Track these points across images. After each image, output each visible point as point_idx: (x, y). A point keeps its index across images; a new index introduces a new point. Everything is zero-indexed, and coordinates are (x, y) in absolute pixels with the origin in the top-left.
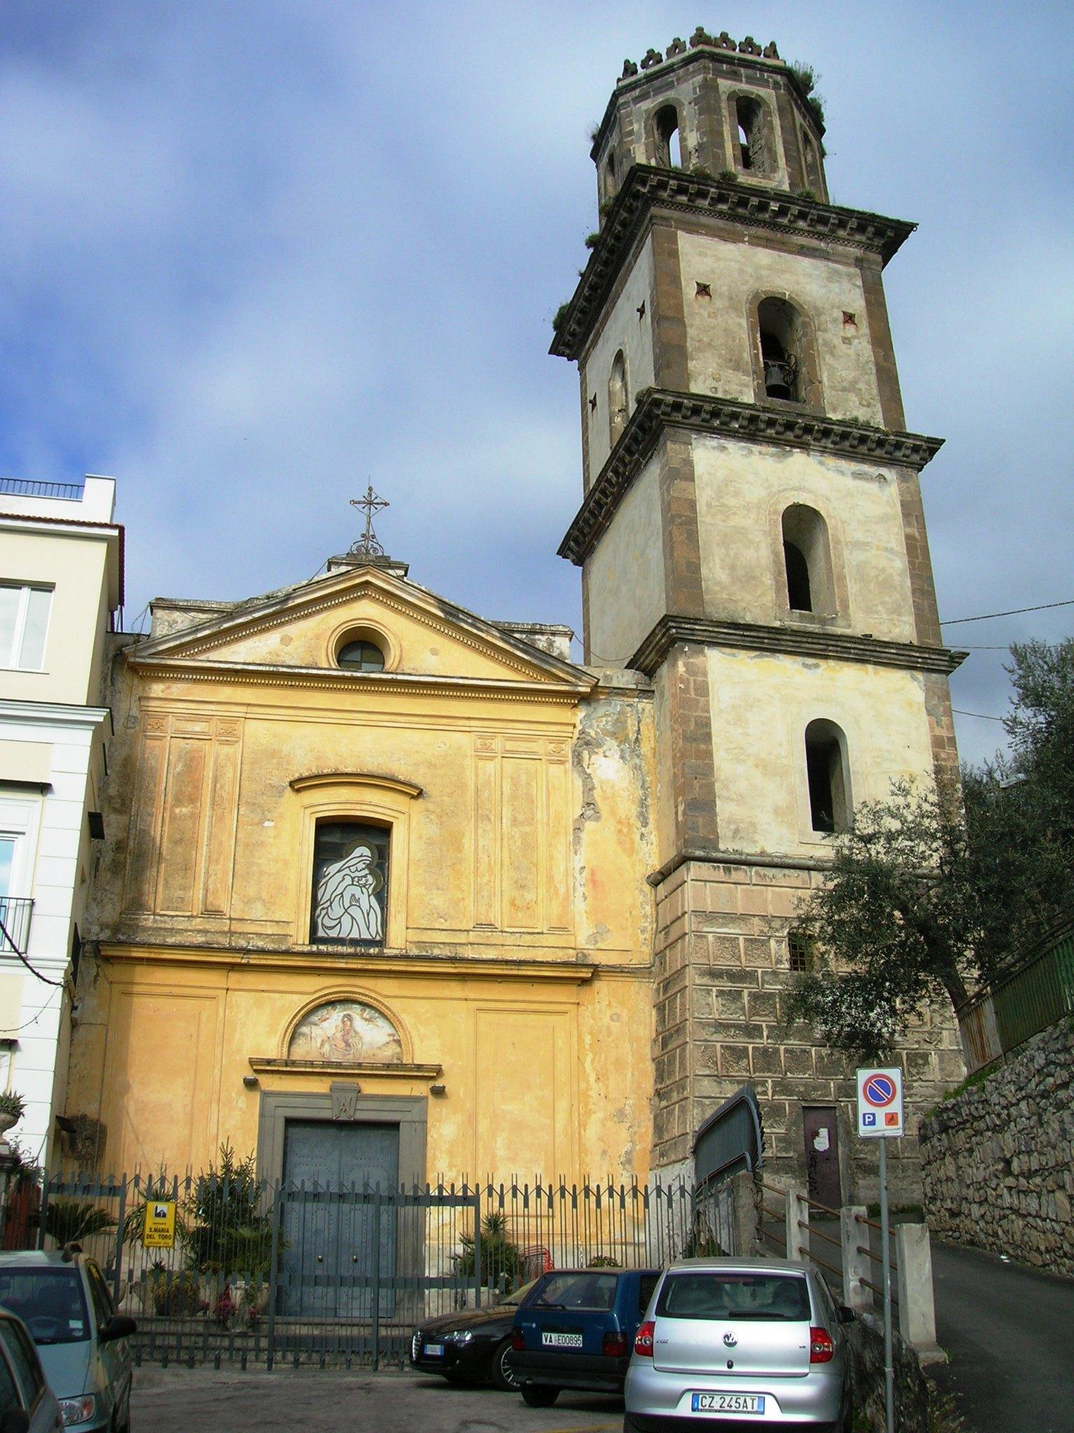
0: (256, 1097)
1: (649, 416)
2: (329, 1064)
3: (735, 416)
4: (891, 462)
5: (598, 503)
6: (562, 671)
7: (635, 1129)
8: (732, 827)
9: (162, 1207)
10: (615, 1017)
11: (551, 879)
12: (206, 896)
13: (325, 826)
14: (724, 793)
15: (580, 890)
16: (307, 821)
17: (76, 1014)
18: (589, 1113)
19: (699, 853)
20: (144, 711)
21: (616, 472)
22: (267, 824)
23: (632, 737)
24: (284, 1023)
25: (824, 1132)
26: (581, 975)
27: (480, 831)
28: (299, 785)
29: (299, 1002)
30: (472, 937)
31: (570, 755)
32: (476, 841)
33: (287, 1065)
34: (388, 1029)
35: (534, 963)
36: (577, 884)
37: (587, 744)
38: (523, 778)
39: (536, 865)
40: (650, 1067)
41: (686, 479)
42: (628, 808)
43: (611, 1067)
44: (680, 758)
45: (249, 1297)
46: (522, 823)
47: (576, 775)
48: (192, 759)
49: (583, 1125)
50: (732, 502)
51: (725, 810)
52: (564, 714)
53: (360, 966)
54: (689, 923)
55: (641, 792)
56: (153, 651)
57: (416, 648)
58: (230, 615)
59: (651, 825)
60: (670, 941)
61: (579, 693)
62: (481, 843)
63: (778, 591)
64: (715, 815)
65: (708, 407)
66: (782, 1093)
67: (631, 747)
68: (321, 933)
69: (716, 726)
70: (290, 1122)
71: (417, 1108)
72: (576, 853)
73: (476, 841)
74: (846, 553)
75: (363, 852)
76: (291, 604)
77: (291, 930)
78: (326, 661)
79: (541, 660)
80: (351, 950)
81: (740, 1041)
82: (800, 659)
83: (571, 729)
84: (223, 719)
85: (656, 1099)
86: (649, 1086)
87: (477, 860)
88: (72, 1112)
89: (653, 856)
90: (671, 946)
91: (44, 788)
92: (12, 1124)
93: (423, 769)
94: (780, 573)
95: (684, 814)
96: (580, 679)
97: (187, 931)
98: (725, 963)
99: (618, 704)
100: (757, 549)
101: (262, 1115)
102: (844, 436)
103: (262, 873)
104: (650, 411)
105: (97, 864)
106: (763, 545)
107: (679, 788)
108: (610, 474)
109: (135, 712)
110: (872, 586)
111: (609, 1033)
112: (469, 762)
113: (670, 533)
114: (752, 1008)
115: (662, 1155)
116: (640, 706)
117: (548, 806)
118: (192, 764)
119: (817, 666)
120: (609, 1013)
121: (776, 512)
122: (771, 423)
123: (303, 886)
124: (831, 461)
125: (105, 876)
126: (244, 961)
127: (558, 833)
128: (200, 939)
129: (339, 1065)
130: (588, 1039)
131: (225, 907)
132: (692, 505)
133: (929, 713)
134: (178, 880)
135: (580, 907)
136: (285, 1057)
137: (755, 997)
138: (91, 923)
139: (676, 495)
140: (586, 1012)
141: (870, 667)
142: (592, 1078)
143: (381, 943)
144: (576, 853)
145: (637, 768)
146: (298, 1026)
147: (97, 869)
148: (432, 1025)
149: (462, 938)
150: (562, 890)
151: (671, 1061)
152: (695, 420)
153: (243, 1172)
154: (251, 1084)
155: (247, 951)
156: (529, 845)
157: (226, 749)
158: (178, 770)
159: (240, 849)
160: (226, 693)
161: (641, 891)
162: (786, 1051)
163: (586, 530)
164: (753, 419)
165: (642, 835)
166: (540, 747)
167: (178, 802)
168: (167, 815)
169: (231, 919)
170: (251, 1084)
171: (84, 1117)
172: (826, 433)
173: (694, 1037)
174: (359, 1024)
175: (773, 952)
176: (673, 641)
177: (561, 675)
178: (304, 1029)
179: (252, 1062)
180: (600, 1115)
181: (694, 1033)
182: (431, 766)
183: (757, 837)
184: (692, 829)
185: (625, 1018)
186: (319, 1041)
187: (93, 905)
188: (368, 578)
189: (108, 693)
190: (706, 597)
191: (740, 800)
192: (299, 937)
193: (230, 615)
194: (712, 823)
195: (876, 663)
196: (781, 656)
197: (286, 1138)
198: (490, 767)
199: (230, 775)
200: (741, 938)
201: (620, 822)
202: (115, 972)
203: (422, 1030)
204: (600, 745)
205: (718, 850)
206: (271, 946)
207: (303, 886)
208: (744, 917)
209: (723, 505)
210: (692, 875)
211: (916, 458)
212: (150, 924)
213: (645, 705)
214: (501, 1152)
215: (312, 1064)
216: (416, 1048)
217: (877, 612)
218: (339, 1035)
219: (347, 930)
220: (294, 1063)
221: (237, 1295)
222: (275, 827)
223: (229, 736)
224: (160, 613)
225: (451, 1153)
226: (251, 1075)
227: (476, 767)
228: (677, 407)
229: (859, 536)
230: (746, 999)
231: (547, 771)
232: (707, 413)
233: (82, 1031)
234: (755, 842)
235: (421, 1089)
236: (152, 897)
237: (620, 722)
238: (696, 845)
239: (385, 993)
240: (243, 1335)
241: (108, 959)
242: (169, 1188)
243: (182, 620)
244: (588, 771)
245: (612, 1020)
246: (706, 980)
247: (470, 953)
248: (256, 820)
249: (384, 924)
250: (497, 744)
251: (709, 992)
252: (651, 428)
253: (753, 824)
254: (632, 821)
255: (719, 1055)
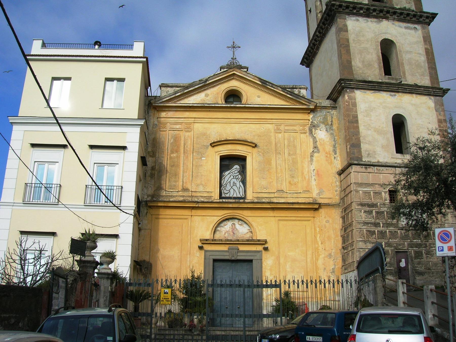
0: (203, 252)
1: (331, 10)
2: (228, 240)
3: (361, 8)
4: (418, 22)
5: (314, 44)
6: (304, 101)
7: (335, 260)
8: (367, 153)
9: (167, 290)
10: (327, 221)
11: (303, 173)
12: (183, 184)
13: (223, 159)
14: (364, 141)
15: (313, 177)
16: (217, 157)
17: (140, 226)
18: (319, 255)
19: (355, 162)
20: (159, 122)
21: (320, 32)
22: (203, 158)
23: (330, 123)
24: (211, 227)
25: (403, 260)
26: (315, 207)
27: (277, 158)
28: (213, 145)
29: (216, 219)
30: (276, 195)
31: (308, 130)
32: (276, 161)
33: (213, 241)
34: (247, 228)
35: (298, 203)
36: (312, 175)
37: (314, 126)
38: (292, 139)
39: (297, 169)
40: (340, 239)
41: (345, 31)
42: (329, 148)
43: (326, 239)
44: (347, 129)
45: (200, 321)
46: (292, 155)
47: (310, 137)
48: (176, 138)
49: (317, 259)
50: (362, 39)
51: (364, 147)
52: (305, 116)
53: (237, 206)
54: (353, 187)
55: (334, 143)
56: (161, 101)
57: (252, 95)
58: (187, 88)
59: (338, 154)
60: (346, 194)
61: (311, 108)
62: (278, 162)
63: (380, 70)
64: (361, 149)
65: (351, 6)
66: (388, 246)
67: (329, 127)
68: (223, 196)
69: (360, 117)
70: (215, 261)
71: (258, 255)
72: (311, 164)
73: (276, 161)
74: (404, 55)
75: (237, 167)
76: (208, 83)
77: (213, 195)
78: (221, 101)
79: (296, 97)
80: (234, 201)
81: (373, 228)
82: (389, 93)
83: (308, 121)
84: (186, 123)
85: (343, 250)
86: (340, 245)
87: (277, 168)
88: (141, 259)
89: (338, 165)
90: (346, 196)
91: (124, 148)
92: (112, 262)
93: (256, 138)
94: (380, 63)
95: (350, 148)
96: (310, 104)
97: (177, 196)
98: (367, 201)
99: (324, 112)
100: (372, 54)
101: (205, 259)
102: (401, 14)
103: (202, 175)
104: (331, 8)
105: (146, 174)
106: (374, 54)
107: (347, 140)
108: (317, 33)
109: (156, 122)
110: (413, 67)
111: (325, 227)
112: (272, 134)
113: (340, 51)
114: (376, 217)
115: (345, 269)
116: (332, 112)
117: (301, 148)
118: (176, 139)
119: (395, 95)
120: (325, 220)
121: (378, 42)
122: (374, 10)
123: (217, 179)
124: (397, 23)
125: (148, 178)
126: (197, 206)
127: (305, 158)
128: (181, 199)
129: (231, 240)
130: (318, 229)
131: (190, 188)
132: (348, 40)
133: (436, 111)
134: (173, 179)
135: (314, 183)
136: (212, 238)
137: (377, 213)
138: (144, 195)
139: (342, 37)
140: (317, 220)
141: (414, 95)
142: (320, 243)
143: (244, 198)
144: (311, 164)
145: (332, 134)
146: (216, 227)
147: (145, 177)
148: (263, 226)
149: (272, 195)
150: (307, 178)
151: (348, 236)
152: (347, 11)
153: (199, 278)
154: (201, 248)
155: (198, 202)
156: (295, 162)
157: (187, 134)
158: (172, 141)
159: (194, 167)
160: (187, 114)
161: (335, 177)
162: (389, 232)
163: (310, 54)
164: (368, 9)
165: (335, 158)
166: (296, 128)
167: (172, 152)
168: (169, 157)
169: (192, 191)
170: (201, 248)
171: (144, 261)
172: (395, 13)
173: (356, 227)
174: (237, 226)
175: (383, 196)
176: (343, 88)
177: (304, 102)
178: (219, 229)
179: (201, 240)
180: (323, 256)
181: (356, 226)
182: (259, 136)
183: (376, 156)
184: (353, 154)
185: (331, 222)
186: (224, 232)
187: (145, 189)
188: (234, 72)
189: (147, 117)
190: (354, 72)
191: (370, 143)
192: (216, 197)
193: (187, 88)
194: (360, 152)
195: (416, 94)
196: (382, 92)
197: (213, 266)
198: (280, 135)
199: (189, 142)
200: (372, 192)
201: (327, 153)
202: (153, 211)
203: (260, 228)
204: (318, 127)
205: (362, 161)
206: (206, 200)
207: (217, 179)
208: (373, 185)
209: (359, 40)
210: (353, 170)
211: (427, 20)
212: (164, 194)
213: (334, 112)
214: (288, 270)
215: (221, 240)
216: (258, 234)
217: (416, 76)
218: (231, 230)
219: (232, 194)
220: (215, 240)
221: (196, 321)
222: (206, 159)
223: (188, 129)
224: (163, 89)
225: (271, 270)
226: (201, 245)
227: (275, 136)
228: (340, 6)
229: (408, 49)
230: (374, 213)
231: (300, 136)
232: (351, 8)
233: (142, 232)
234: (375, 158)
235: (260, 248)
236: (165, 185)
237: (325, 118)
238: (354, 160)
239: (246, 215)
240: (198, 335)
241: (150, 207)
242: (168, 284)
243: (171, 90)
244: (315, 136)
245: (326, 222)
246: (360, 207)
247: (275, 200)
248: (199, 157)
249: (245, 191)
250: (282, 127)
251: (361, 211)
252: (331, 14)
253: (374, 152)
254: (331, 153)
255: (365, 234)
